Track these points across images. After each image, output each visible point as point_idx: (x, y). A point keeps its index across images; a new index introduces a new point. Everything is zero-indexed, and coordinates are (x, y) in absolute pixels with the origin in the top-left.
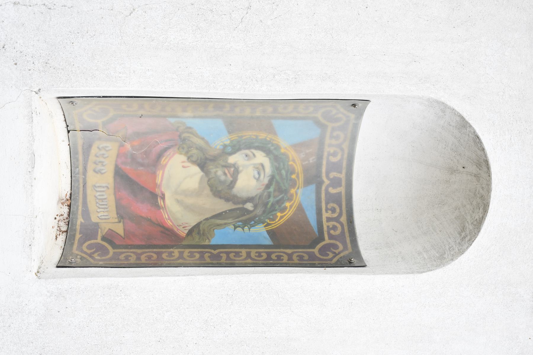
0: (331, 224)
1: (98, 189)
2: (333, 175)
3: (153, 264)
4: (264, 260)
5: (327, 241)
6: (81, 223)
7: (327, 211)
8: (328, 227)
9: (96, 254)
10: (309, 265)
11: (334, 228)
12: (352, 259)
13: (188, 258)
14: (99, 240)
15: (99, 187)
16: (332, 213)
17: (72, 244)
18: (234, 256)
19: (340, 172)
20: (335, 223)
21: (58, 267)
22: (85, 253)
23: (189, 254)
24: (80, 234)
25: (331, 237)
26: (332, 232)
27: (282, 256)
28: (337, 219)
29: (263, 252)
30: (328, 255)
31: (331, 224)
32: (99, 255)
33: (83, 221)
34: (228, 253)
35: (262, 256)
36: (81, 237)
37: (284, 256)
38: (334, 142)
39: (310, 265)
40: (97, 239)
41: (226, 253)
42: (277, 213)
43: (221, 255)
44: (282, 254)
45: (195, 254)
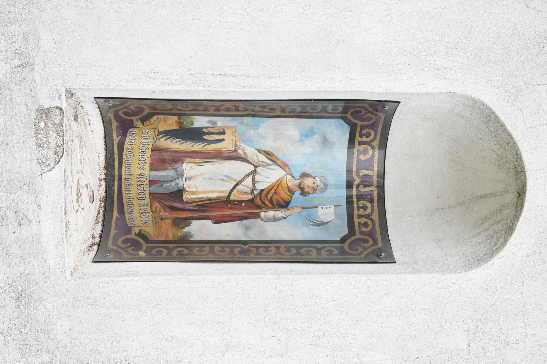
0: (363, 220)
1: (126, 180)
2: (363, 172)
3: (162, 259)
4: (274, 254)
5: (358, 236)
6: (117, 217)
7: (358, 209)
8: (359, 223)
9: (131, 248)
10: (212, 258)
11: (366, 225)
12: (382, 254)
13: (263, 253)
14: (133, 236)
15: (127, 179)
16: (364, 211)
17: (107, 240)
18: (264, 251)
19: (372, 170)
20: (366, 220)
21: (94, 262)
22: (120, 247)
23: (220, 249)
24: (115, 230)
25: (362, 233)
26: (363, 229)
27: (312, 251)
28: (368, 216)
29: (293, 247)
30: (357, 250)
31: (363, 220)
32: (133, 250)
33: (118, 215)
34: (257, 248)
35: (225, 251)
36: (116, 233)
37: (284, 252)
38: (364, 139)
39: (153, 260)
40: (131, 234)
41: (255, 247)
42: (260, 213)
43: (251, 249)
44: (310, 249)
45: (292, 249)
